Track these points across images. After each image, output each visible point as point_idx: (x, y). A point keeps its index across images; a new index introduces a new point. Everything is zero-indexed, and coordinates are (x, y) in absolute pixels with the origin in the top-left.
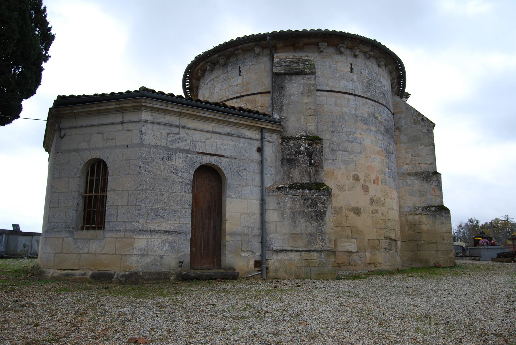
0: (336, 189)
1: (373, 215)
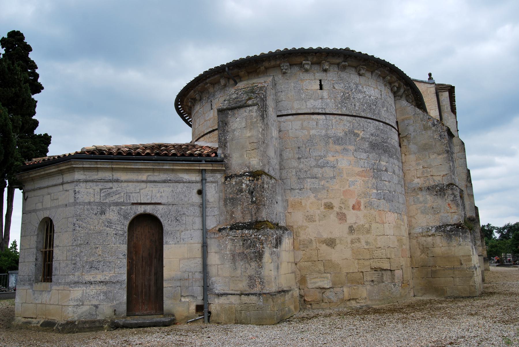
0: (304, 221)
1: (353, 245)
